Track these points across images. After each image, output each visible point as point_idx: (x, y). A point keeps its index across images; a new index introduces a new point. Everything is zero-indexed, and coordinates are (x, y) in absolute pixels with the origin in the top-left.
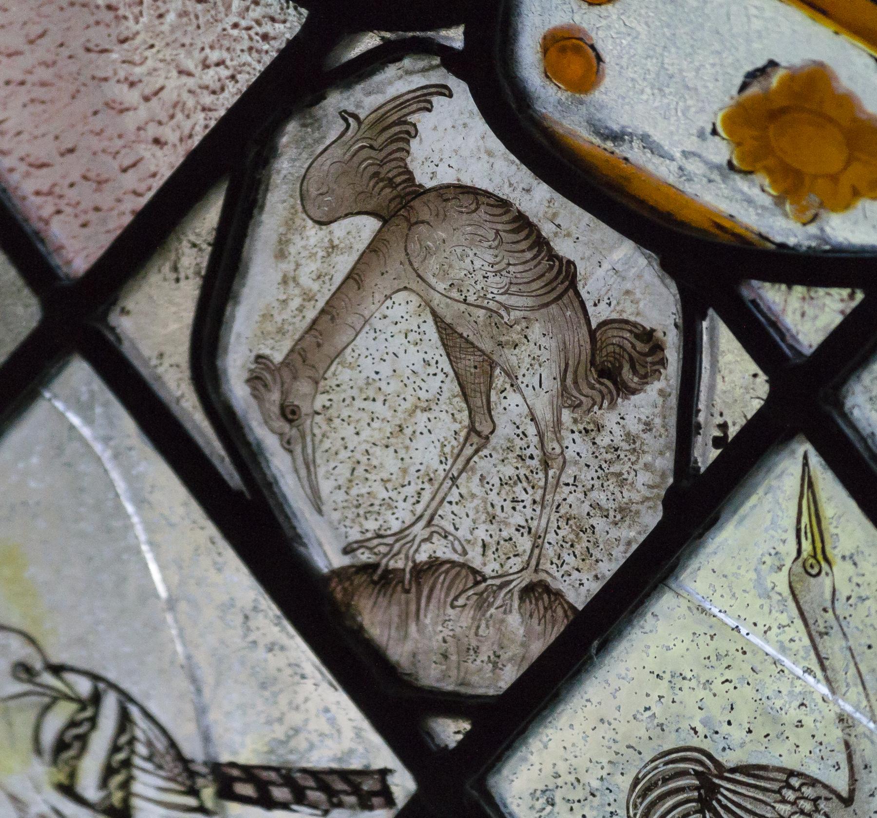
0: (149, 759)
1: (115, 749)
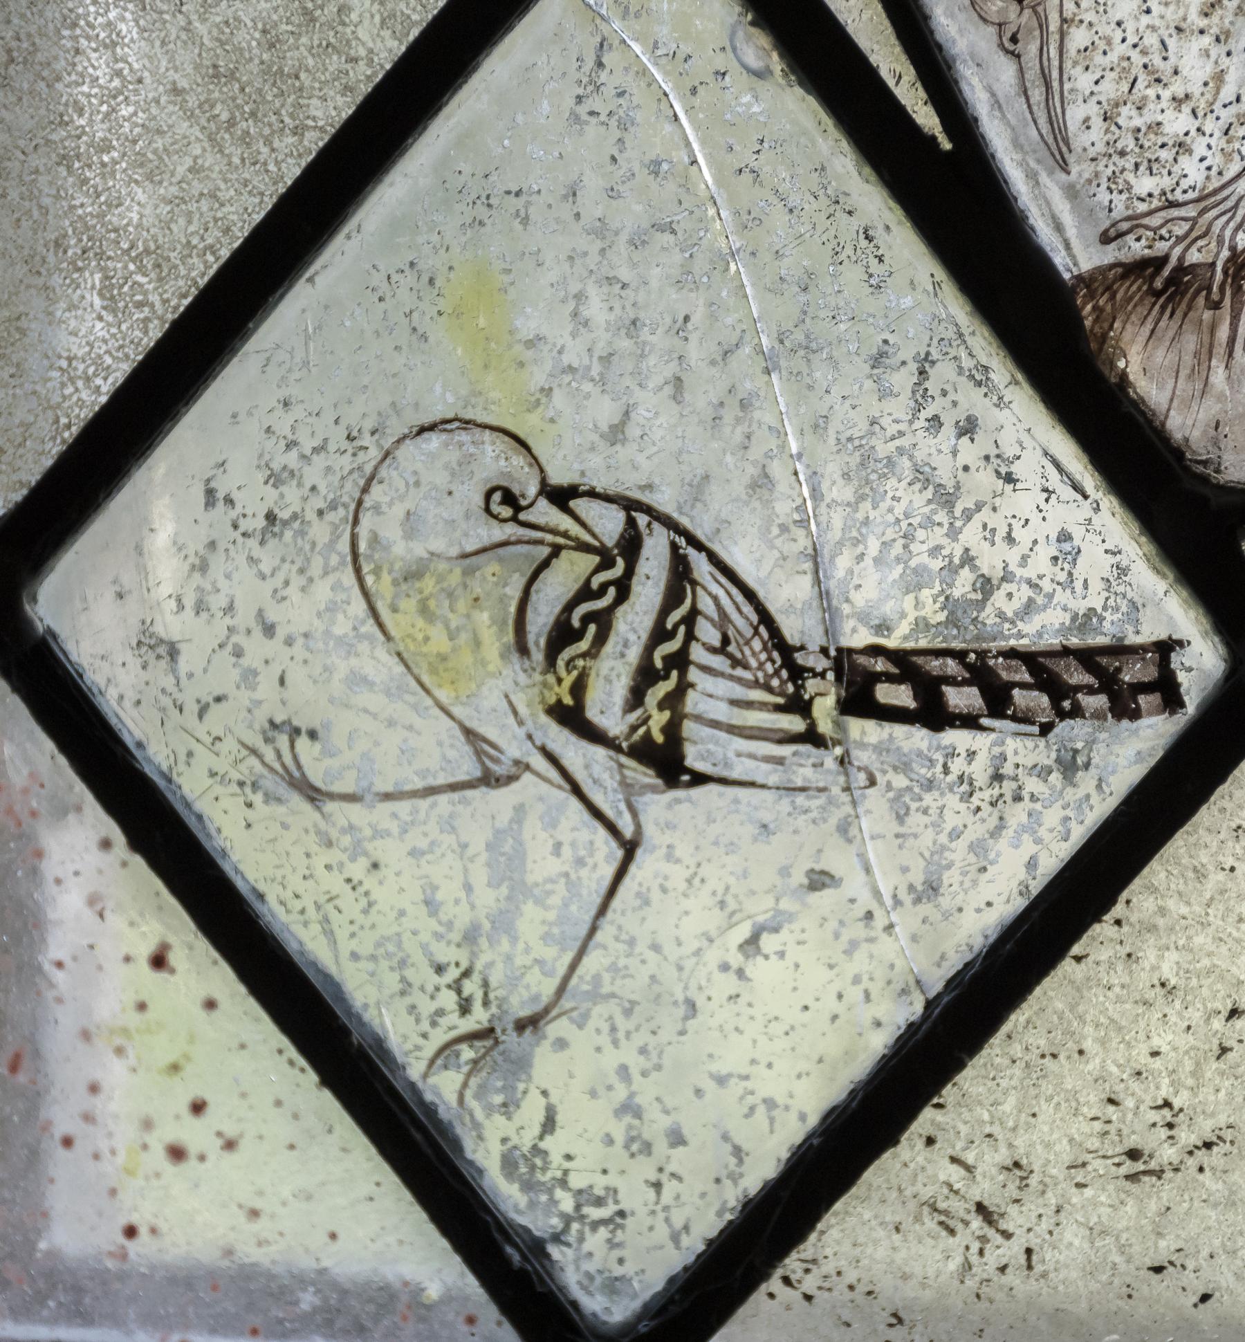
0: (722, 649)
1: (660, 634)
